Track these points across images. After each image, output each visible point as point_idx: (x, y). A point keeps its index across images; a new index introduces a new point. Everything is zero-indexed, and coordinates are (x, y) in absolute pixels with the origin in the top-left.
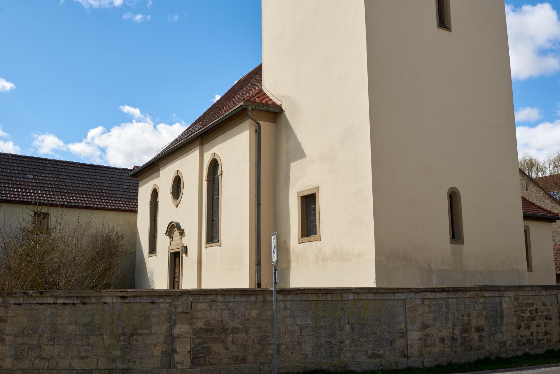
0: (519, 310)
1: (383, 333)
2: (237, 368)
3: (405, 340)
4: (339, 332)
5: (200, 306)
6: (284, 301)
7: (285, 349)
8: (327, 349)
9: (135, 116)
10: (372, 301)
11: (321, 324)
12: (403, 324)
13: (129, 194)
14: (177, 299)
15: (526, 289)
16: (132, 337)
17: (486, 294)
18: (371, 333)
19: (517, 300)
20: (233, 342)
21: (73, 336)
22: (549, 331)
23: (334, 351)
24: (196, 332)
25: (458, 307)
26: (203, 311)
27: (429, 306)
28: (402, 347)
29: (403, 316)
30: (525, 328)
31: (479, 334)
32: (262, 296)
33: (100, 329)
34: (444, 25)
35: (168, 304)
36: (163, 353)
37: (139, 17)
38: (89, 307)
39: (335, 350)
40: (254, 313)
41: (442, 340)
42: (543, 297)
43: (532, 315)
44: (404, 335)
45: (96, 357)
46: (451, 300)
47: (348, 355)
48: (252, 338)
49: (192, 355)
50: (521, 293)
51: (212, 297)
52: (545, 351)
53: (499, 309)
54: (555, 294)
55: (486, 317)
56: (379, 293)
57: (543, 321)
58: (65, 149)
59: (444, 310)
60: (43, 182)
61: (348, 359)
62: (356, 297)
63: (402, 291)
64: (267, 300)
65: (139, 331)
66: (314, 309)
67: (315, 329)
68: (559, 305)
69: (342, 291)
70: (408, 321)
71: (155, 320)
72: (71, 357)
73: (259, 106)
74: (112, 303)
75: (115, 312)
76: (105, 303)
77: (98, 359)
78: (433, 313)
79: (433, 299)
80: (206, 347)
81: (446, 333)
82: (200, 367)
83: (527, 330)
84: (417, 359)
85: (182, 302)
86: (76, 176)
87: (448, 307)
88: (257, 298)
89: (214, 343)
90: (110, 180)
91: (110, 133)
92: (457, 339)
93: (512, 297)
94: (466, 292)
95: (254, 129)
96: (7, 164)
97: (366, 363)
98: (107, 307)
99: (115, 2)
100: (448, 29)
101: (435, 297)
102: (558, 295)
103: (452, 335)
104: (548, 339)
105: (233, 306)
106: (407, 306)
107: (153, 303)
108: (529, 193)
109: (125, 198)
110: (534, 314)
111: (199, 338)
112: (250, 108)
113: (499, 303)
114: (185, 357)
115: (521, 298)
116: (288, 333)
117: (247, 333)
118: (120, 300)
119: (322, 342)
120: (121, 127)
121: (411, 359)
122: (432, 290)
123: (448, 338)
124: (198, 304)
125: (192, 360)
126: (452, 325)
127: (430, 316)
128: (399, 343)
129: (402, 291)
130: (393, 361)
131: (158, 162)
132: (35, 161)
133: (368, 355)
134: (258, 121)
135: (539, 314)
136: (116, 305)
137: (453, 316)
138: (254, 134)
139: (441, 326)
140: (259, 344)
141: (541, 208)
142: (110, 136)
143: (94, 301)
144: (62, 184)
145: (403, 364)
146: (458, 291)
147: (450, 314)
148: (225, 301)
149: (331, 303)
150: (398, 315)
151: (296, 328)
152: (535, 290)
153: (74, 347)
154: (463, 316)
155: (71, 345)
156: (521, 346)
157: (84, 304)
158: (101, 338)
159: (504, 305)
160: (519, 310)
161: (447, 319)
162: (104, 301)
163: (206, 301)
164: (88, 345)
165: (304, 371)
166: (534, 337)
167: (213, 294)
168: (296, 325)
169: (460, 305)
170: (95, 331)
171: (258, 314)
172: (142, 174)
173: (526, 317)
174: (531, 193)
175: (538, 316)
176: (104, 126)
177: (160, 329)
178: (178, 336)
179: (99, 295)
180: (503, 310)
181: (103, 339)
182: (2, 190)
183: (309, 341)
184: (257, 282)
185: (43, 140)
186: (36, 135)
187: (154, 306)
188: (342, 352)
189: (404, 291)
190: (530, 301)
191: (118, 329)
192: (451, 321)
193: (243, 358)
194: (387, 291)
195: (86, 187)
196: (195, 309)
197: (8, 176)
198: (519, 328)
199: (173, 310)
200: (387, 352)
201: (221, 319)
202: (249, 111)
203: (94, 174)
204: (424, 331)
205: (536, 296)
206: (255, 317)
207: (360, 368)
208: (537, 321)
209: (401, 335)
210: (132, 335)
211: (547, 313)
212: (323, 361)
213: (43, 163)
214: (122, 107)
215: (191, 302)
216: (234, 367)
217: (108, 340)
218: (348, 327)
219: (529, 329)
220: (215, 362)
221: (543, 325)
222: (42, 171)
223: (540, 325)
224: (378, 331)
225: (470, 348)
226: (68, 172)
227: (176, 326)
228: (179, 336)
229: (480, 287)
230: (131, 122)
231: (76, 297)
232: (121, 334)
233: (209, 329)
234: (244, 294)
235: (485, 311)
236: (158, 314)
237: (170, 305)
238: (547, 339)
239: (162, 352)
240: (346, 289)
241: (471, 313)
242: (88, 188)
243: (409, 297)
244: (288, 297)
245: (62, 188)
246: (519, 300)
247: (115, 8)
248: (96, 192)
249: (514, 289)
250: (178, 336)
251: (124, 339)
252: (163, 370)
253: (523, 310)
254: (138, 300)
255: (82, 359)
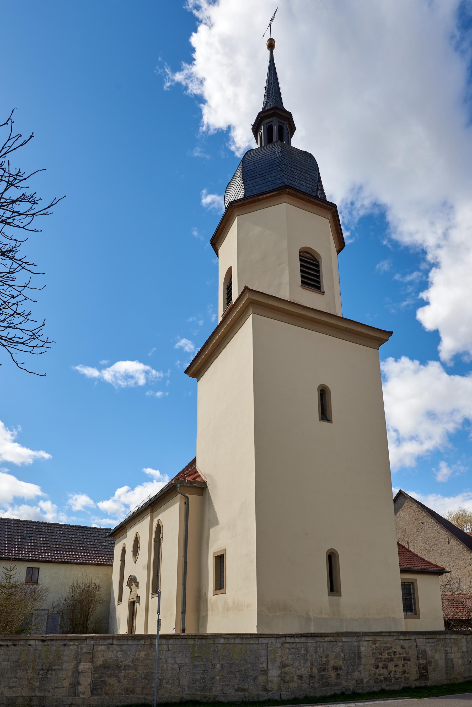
0: (377, 653)
1: (248, 671)
2: (126, 698)
3: (266, 677)
4: (211, 670)
5: (100, 648)
6: (167, 644)
7: (166, 683)
8: (201, 683)
9: (155, 476)
10: (239, 644)
11: (196, 663)
12: (265, 663)
13: (109, 550)
14: (83, 643)
15: (383, 634)
16: (48, 672)
17: (344, 639)
18: (237, 671)
19: (375, 644)
20: (124, 677)
21: (5, 670)
22: (407, 670)
23: (206, 685)
24: (96, 668)
25: (317, 650)
26: (102, 652)
27: (289, 649)
28: (264, 682)
29: (265, 657)
30: (383, 668)
31: (336, 673)
32: (149, 641)
33: (25, 665)
34: (327, 418)
35: (76, 646)
36: (70, 684)
37: (159, 394)
38: (18, 648)
39: (207, 684)
40: (142, 654)
41: (300, 677)
42: (402, 642)
43: (390, 657)
44: (266, 672)
45: (21, 687)
46: (309, 644)
47: (218, 689)
48: (140, 674)
49: (92, 687)
50: (378, 638)
51: (109, 641)
52: (402, 687)
53: (357, 651)
54: (414, 639)
55: (344, 659)
56: (246, 638)
57: (401, 663)
58: (94, 507)
59: (303, 652)
60: (37, 542)
61: (218, 691)
62: (226, 641)
63: (264, 636)
64: (153, 643)
65: (53, 667)
66: (192, 651)
67: (191, 667)
68: (418, 648)
69: (214, 636)
70: (269, 661)
71: (65, 659)
72: (3, 686)
73: (187, 483)
74: (35, 645)
75: (37, 652)
76: (30, 645)
77: (23, 688)
78: (292, 655)
79: (293, 643)
80: (103, 681)
81: (304, 671)
82: (98, 696)
83: (384, 670)
84: (276, 693)
85: (86, 644)
86: (65, 536)
87: (306, 650)
88: (145, 642)
89: (109, 677)
90: (94, 539)
91: (134, 491)
92: (314, 677)
93: (371, 642)
94: (324, 637)
95: (183, 501)
96: (9, 527)
97: (233, 695)
98: (31, 648)
99: (139, 382)
100: (330, 421)
101: (294, 642)
102: (417, 639)
103: (310, 673)
104: (406, 678)
105: (126, 648)
106: (269, 649)
107: (65, 645)
108: (451, 547)
109: (105, 554)
110: (392, 656)
111: (98, 673)
112: (179, 485)
113: (358, 646)
114: (86, 688)
115: (379, 642)
116: (169, 670)
117: (136, 670)
118: (41, 643)
119: (196, 678)
120: (143, 486)
121: (271, 693)
122: (290, 636)
123: (306, 676)
124: (99, 646)
125: (91, 691)
126: (310, 665)
127: (289, 657)
128: (261, 679)
129: (264, 636)
130: (255, 694)
131: (126, 525)
132: (33, 524)
133: (235, 689)
134: (186, 495)
135: (398, 656)
136: (38, 646)
137: (312, 657)
138: (184, 506)
139: (300, 665)
140: (146, 678)
141: (430, 563)
142: (134, 493)
143: (22, 643)
144: (53, 543)
145: (264, 696)
146: (316, 636)
147: (308, 655)
148: (120, 644)
149: (205, 646)
150: (261, 656)
151: (176, 666)
152: (393, 635)
153: (6, 679)
154: (321, 657)
155: (4, 677)
156: (378, 683)
157: (15, 645)
158: (26, 672)
159: (363, 649)
160: (377, 653)
161: (306, 660)
162: (29, 643)
163: (104, 644)
164: (16, 677)
165: (181, 701)
166: (392, 676)
167: (110, 639)
168: (176, 663)
169: (318, 649)
170: (21, 666)
171: (145, 655)
172: (117, 534)
173: (384, 658)
174: (453, 546)
175: (396, 657)
176: (129, 486)
177: (69, 666)
178: (82, 672)
179: (25, 638)
180: (361, 653)
181: (27, 673)
182: (2, 550)
183: (186, 676)
184: (182, 627)
185: (76, 499)
186: (70, 495)
187: (66, 648)
188: (213, 686)
189: (266, 636)
190: (389, 645)
191: (38, 665)
192: (309, 661)
193: (132, 689)
194: (252, 637)
195: (73, 546)
196: (96, 650)
197: (8, 537)
198: (377, 667)
199: (80, 650)
200: (251, 687)
201: (116, 658)
202: (178, 487)
203: (81, 534)
204: (283, 670)
205: (394, 641)
206: (143, 657)
207: (227, 699)
208: (395, 662)
209: (263, 673)
210: (48, 670)
211: (406, 655)
212: (197, 693)
213: (39, 526)
214: (145, 469)
215: (93, 645)
216: (125, 696)
217: (30, 674)
218: (218, 666)
219: (387, 669)
220: (110, 692)
221: (401, 666)
222: (38, 533)
223: (398, 665)
224: (243, 669)
225: (328, 685)
226: (59, 533)
227: (81, 664)
228: (83, 672)
229: (338, 633)
230: (153, 482)
231: (9, 640)
232: (40, 669)
233: (106, 666)
234: (135, 639)
235: (343, 653)
236: (68, 654)
237: (77, 647)
238: (405, 677)
239: (70, 683)
240: (218, 635)
241: (329, 655)
242: (75, 546)
243: (270, 641)
244: (171, 641)
245: (52, 547)
246: (377, 644)
247: (139, 387)
248: (81, 549)
249: (371, 635)
250: (82, 672)
251: (42, 673)
252: (69, 698)
253: (381, 652)
254: (54, 643)
255: (11, 688)
